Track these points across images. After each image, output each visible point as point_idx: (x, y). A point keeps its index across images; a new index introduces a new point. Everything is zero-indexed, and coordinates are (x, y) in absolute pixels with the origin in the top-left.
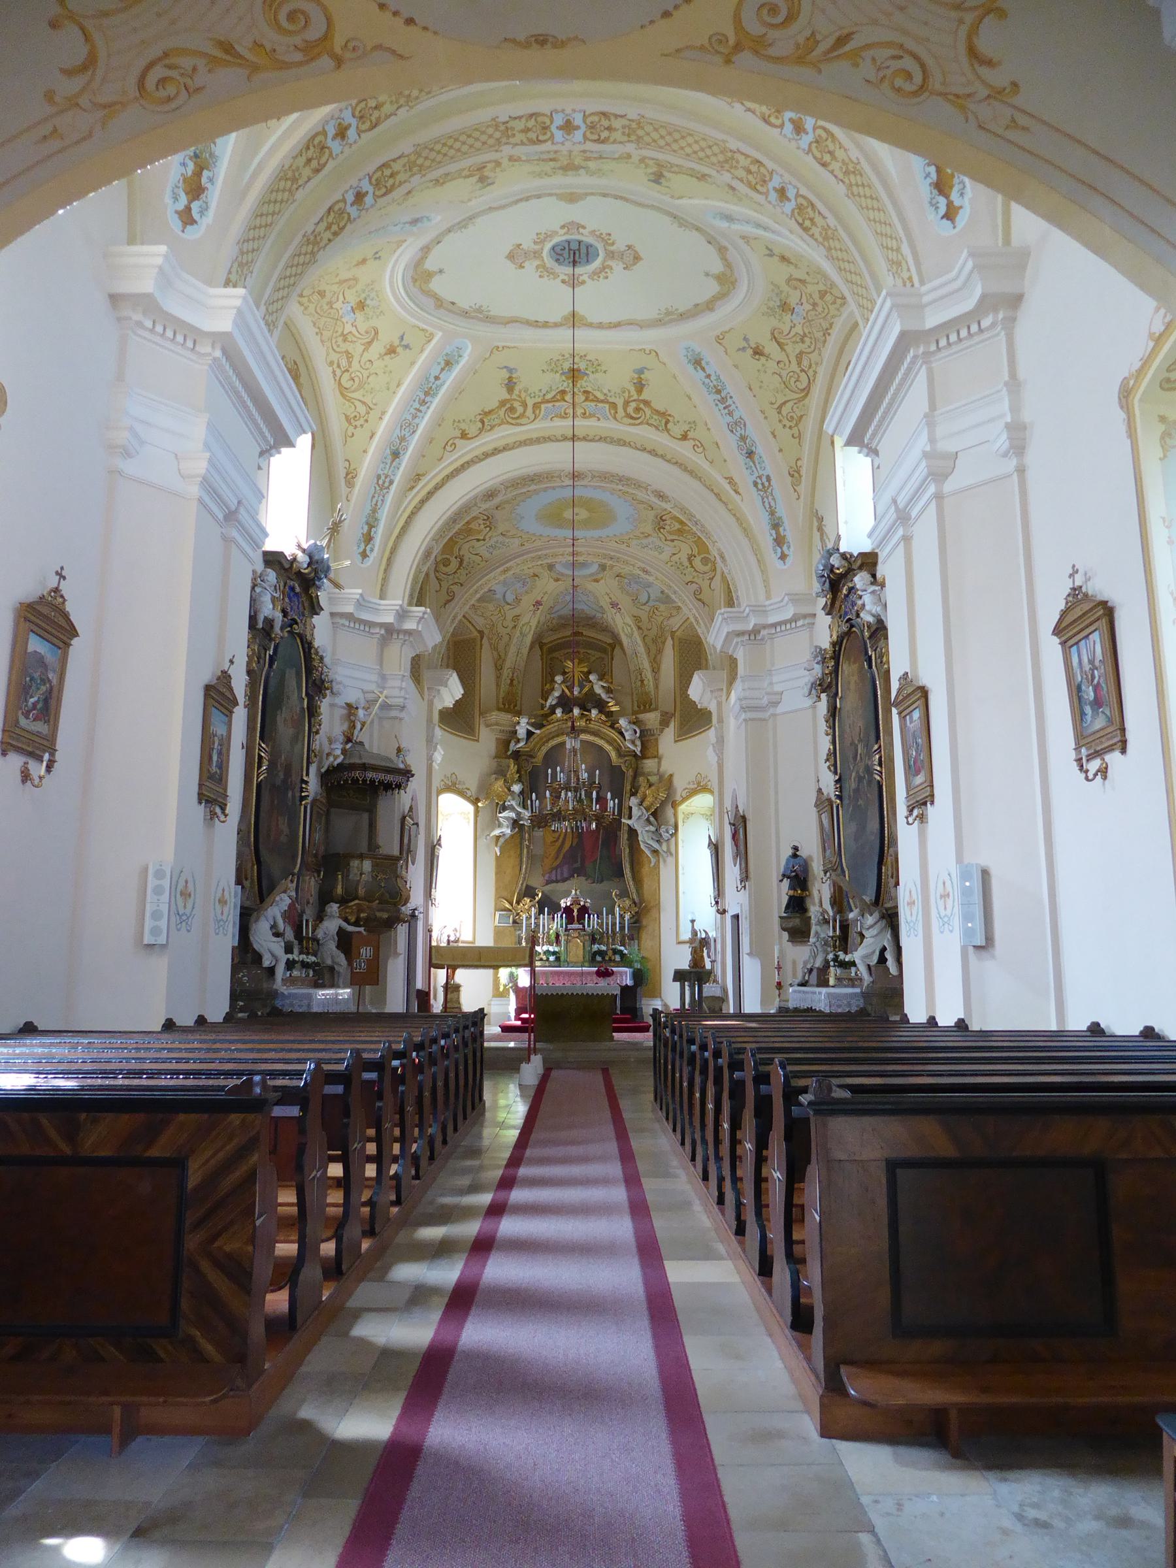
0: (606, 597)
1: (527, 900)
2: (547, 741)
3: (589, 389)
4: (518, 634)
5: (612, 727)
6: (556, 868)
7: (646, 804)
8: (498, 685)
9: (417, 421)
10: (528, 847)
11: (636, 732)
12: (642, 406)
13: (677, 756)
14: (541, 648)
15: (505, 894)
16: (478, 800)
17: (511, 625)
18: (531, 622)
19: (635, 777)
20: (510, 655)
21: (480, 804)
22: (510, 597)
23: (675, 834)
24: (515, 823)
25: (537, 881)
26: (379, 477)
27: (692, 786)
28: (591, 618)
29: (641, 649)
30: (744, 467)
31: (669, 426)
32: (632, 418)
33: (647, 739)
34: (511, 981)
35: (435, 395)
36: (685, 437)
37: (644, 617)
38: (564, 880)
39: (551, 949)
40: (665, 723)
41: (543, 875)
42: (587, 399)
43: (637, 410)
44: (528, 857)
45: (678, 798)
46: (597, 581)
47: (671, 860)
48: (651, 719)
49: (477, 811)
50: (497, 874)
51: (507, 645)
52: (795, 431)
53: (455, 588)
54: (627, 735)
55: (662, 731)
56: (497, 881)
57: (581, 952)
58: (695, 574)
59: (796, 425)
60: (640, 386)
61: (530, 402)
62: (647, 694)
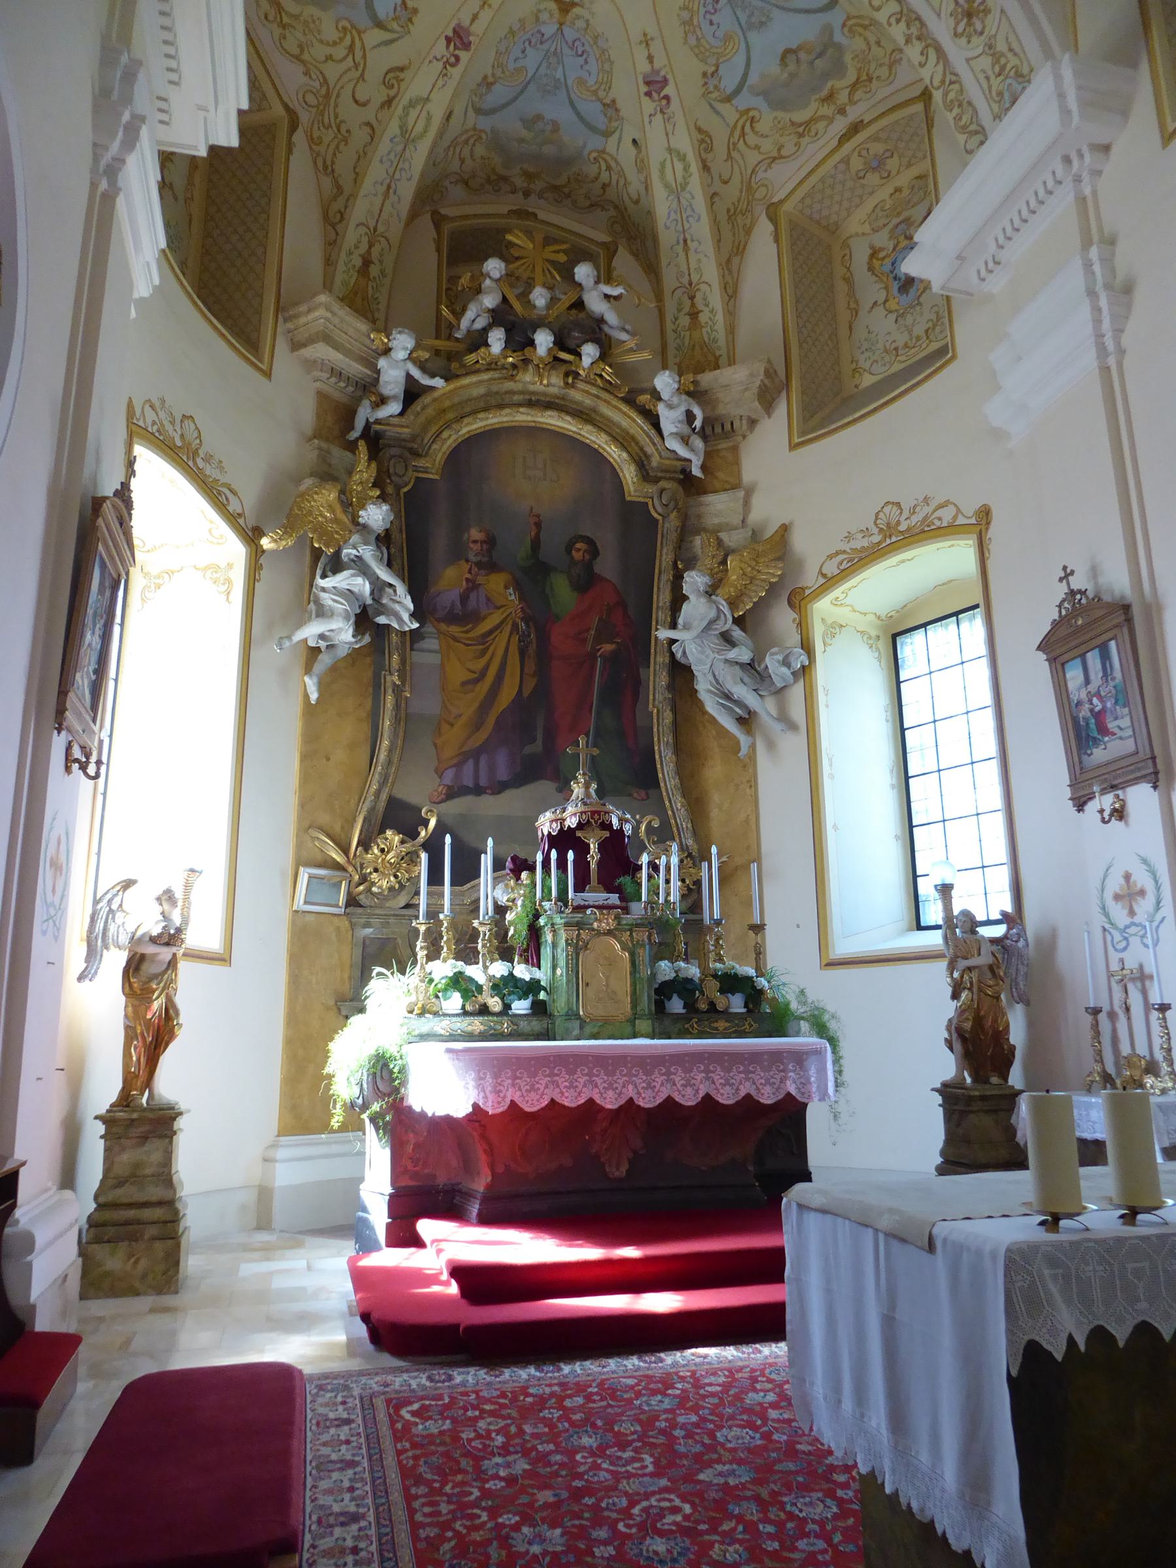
0: (641, 54)
1: (393, 837)
4: (393, 128)
5: (630, 400)
6: (476, 754)
7: (727, 590)
10: (397, 691)
15: (325, 819)
17: (382, 95)
21: (266, 543)
23: (805, 672)
24: (364, 620)
25: (419, 788)
27: (860, 543)
29: (702, 229)
33: (716, 432)
34: (378, 1094)
38: (499, 788)
39: (522, 972)
40: (767, 399)
41: (440, 773)
44: (397, 720)
45: (810, 579)
47: (792, 745)
49: (256, 560)
50: (305, 757)
51: (363, 155)
54: (670, 419)
55: (753, 423)
56: (306, 778)
57: (622, 986)
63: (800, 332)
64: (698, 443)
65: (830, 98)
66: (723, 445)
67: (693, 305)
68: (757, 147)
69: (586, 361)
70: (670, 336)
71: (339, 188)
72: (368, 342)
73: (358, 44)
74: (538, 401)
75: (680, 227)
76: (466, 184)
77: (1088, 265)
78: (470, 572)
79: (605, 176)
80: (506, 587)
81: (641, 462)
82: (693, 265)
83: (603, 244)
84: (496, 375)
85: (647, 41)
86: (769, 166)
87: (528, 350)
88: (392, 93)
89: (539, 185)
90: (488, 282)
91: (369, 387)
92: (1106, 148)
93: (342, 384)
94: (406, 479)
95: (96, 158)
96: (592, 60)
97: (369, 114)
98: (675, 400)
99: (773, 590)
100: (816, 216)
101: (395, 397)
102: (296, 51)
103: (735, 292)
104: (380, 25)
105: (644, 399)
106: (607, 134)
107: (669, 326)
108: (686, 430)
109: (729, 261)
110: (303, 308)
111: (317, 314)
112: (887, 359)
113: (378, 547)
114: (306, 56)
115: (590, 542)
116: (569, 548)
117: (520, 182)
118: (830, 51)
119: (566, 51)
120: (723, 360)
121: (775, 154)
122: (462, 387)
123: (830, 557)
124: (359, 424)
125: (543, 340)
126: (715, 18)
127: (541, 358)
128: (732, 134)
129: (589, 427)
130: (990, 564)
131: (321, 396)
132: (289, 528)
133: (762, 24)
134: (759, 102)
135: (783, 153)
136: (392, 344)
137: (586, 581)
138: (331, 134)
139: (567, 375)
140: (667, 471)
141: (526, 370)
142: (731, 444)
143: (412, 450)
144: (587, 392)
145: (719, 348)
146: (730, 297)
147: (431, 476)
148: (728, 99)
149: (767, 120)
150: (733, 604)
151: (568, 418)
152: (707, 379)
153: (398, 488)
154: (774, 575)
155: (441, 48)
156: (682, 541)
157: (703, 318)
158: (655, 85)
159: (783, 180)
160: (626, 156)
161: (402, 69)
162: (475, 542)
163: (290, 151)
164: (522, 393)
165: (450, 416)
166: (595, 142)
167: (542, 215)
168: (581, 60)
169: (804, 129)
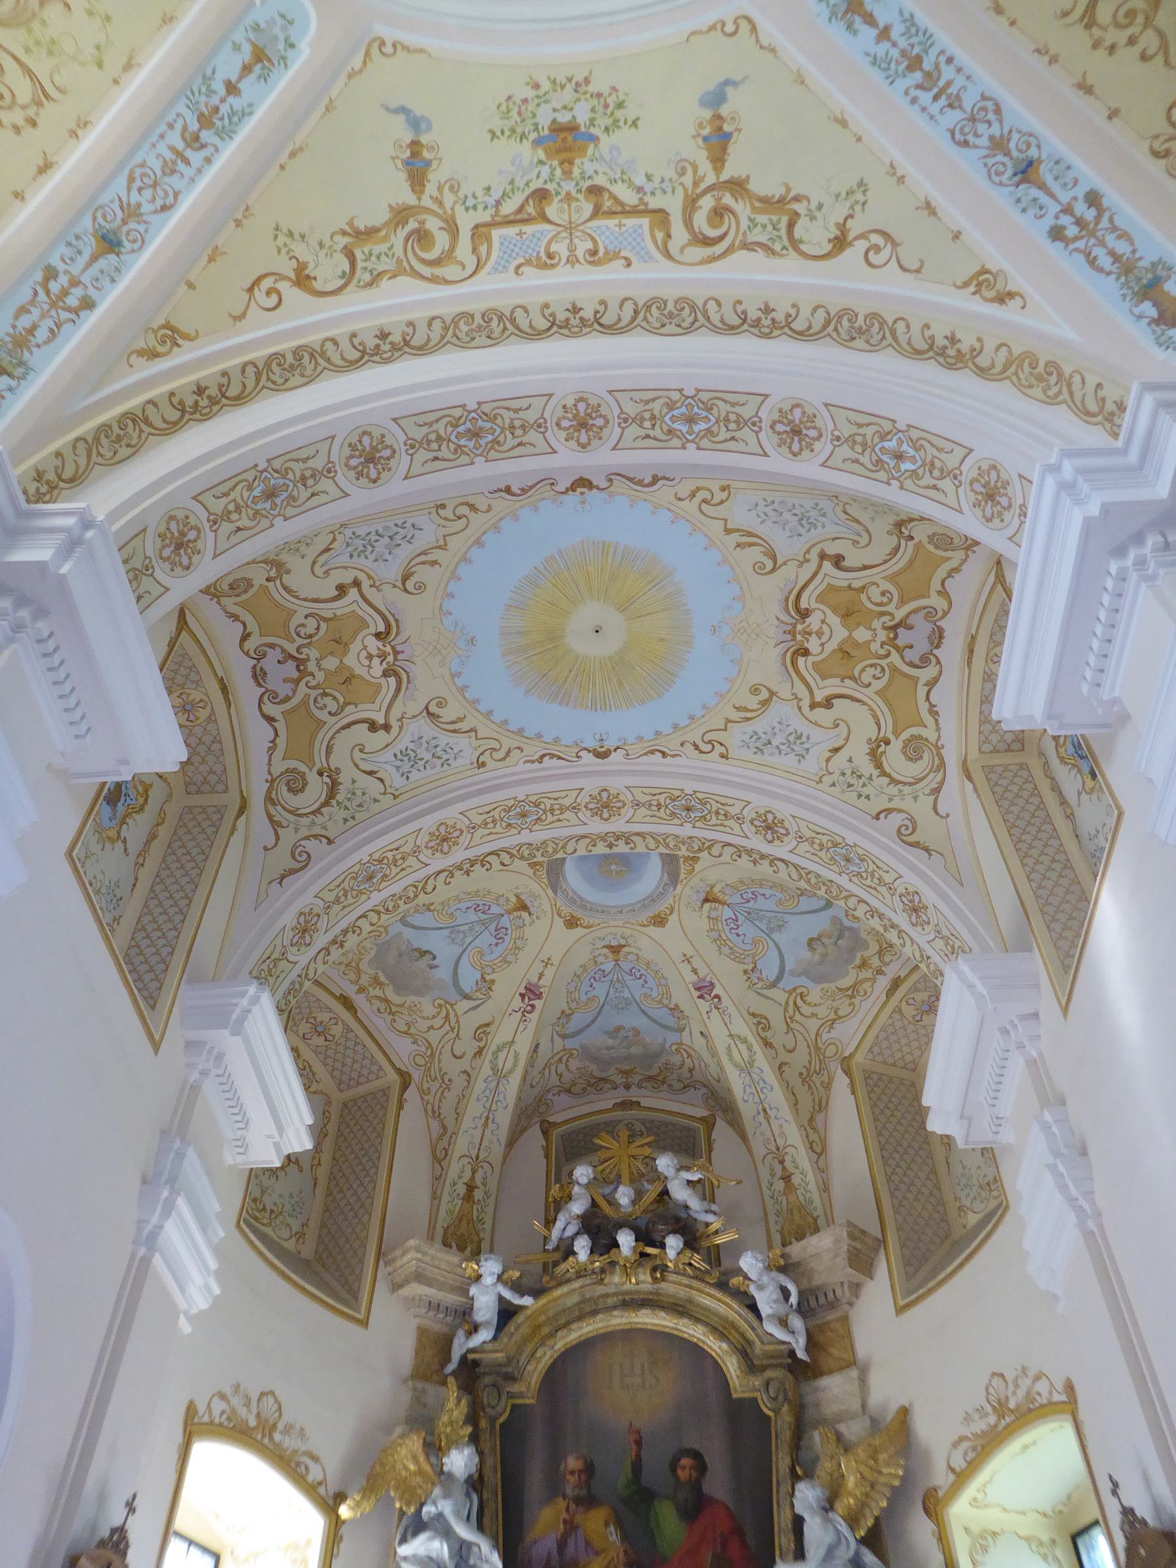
0: (686, 969)
2: (553, 1334)
3: (600, 181)
4: (486, 1071)
5: (722, 1285)
7: (847, 1502)
8: (435, 1196)
9: (174, 181)
11: (786, 1294)
12: (728, 199)
13: (910, 1356)
14: (545, 1133)
16: (340, 1497)
17: (472, 1047)
18: (517, 1038)
19: (799, 1431)
20: (467, 1122)
21: (344, 1511)
22: (469, 978)
26: (51, 274)
27: (980, 1426)
28: (656, 1056)
29: (777, 1097)
30: (1014, 213)
31: (798, 232)
32: (707, 242)
33: (815, 1305)
35: (226, 134)
36: (840, 242)
37: (776, 1018)
40: (862, 1259)
42: (597, 212)
43: (719, 213)
45: (941, 1478)
46: (659, 921)
48: (824, 1250)
51: (462, 1097)
52: (1149, 41)
53: (311, 846)
54: (766, 1302)
55: (856, 1288)
58: (893, 790)
59: (1148, 23)
60: (719, 142)
61: (466, 222)
62: (801, 1208)
63: (889, 1180)
64: (797, 1322)
65: (864, 964)
66: (831, 1316)
67: (784, 1169)
68: (814, 1015)
69: (671, 1253)
70: (769, 1202)
71: (444, 1127)
72: (459, 1271)
73: (452, 1014)
74: (632, 1300)
75: (757, 1099)
76: (569, 1091)
77: (1046, 1128)
78: (567, 1510)
79: (688, 1061)
80: (607, 1524)
81: (744, 1352)
82: (777, 1131)
83: (702, 1119)
84: (588, 1281)
85: (688, 960)
86: (831, 1026)
87: (614, 1250)
88: (482, 1044)
89: (636, 1079)
90: (576, 1189)
91: (464, 1316)
92: (1036, 1016)
93: (441, 1316)
94: (499, 1409)
95: (139, 1230)
96: (649, 979)
97: (465, 1064)
98: (765, 1279)
99: (899, 1496)
100: (890, 1060)
101: (486, 1324)
102: (405, 1029)
103: (824, 1148)
104: (467, 997)
105: (735, 1281)
106: (681, 1030)
107: (766, 1192)
108: (782, 1309)
109: (811, 1119)
110: (398, 1253)
111: (409, 1256)
112: (983, 1195)
113: (468, 1495)
114: (413, 1030)
115: (697, 1456)
116: (673, 1467)
117: (618, 1079)
118: (847, 934)
119: (627, 978)
120: (821, 1222)
121: (832, 1016)
122: (555, 1300)
123: (955, 1445)
124: (456, 1354)
125: (626, 1240)
126: (740, 931)
127: (626, 1259)
128: (786, 1010)
129: (686, 1321)
130: (1089, 1452)
131: (422, 1332)
132: (369, 1490)
133: (780, 927)
134: (804, 981)
135: (840, 1013)
136: (482, 1271)
137: (695, 1506)
138: (437, 1084)
139: (654, 1269)
140: (773, 1357)
141: (612, 1273)
142: (839, 1314)
143: (508, 1375)
144: (680, 1284)
145: (815, 1209)
146: (819, 1155)
147: (527, 1401)
148: (774, 985)
149: (815, 993)
150: (853, 1521)
151: (663, 1314)
152: (796, 1250)
153: (492, 1420)
154: (895, 1476)
155: (517, 1002)
156: (799, 1439)
157: (796, 1180)
158: (704, 989)
159: (849, 1035)
160: (699, 1043)
161: (487, 1025)
162: (572, 1473)
163: (400, 1107)
164: (616, 1294)
165: (546, 1330)
166: (672, 1038)
167: (645, 1102)
168: (641, 981)
169: (852, 992)
